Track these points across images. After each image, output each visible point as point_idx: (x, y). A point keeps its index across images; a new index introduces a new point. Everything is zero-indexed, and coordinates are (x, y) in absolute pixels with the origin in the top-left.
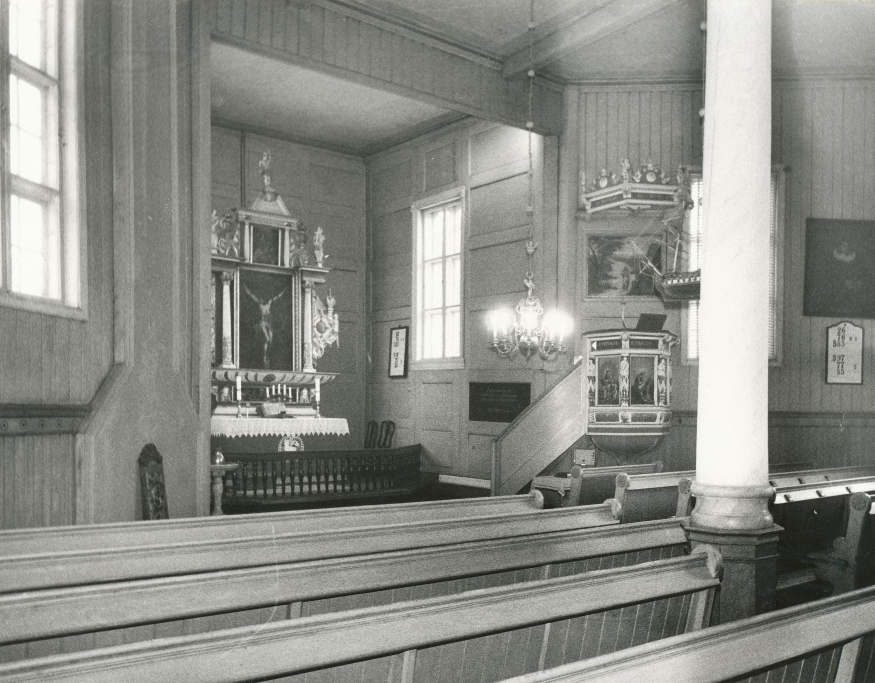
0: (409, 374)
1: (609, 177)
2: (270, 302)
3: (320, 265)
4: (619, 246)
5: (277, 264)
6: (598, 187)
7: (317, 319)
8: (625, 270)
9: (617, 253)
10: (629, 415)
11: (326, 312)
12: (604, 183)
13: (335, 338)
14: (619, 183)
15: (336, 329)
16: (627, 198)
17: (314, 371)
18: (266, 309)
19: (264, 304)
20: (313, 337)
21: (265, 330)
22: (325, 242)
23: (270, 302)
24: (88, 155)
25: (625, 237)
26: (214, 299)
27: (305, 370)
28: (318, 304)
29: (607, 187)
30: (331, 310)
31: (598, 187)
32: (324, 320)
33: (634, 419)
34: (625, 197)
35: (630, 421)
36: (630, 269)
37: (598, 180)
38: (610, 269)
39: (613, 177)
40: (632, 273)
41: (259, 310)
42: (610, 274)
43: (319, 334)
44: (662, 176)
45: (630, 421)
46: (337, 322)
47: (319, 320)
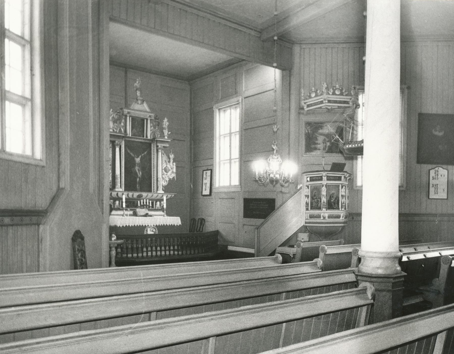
0: (212, 194)
1: (316, 92)
2: (140, 156)
3: (166, 138)
4: (321, 127)
5: (144, 137)
6: (310, 97)
7: (165, 166)
8: (325, 140)
9: (320, 131)
10: (326, 215)
11: (169, 162)
12: (313, 95)
13: (174, 175)
14: (321, 95)
15: (175, 170)
16: (325, 103)
17: (163, 192)
18: (138, 160)
19: (137, 158)
20: (162, 175)
21: (137, 171)
22: (168, 125)
23: (140, 156)
24: (45, 80)
25: (324, 123)
26: (111, 155)
27: (158, 192)
28: (165, 158)
29: (315, 97)
30: (172, 160)
31: (310, 97)
32: (168, 166)
33: (329, 217)
34: (324, 102)
35: (327, 218)
36: (327, 140)
37: (310, 93)
38: (317, 140)
39: (318, 92)
40: (328, 141)
41: (134, 161)
42: (317, 142)
43: (166, 173)
44: (344, 91)
45: (327, 218)
46: (175, 167)
47: (165, 166)
